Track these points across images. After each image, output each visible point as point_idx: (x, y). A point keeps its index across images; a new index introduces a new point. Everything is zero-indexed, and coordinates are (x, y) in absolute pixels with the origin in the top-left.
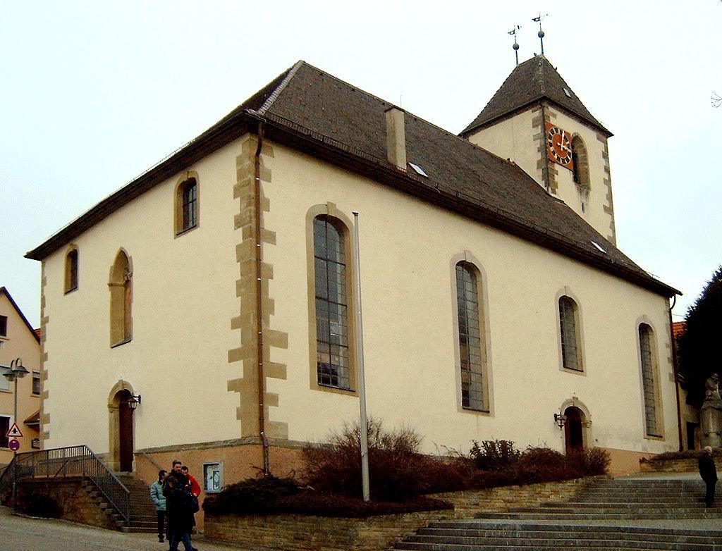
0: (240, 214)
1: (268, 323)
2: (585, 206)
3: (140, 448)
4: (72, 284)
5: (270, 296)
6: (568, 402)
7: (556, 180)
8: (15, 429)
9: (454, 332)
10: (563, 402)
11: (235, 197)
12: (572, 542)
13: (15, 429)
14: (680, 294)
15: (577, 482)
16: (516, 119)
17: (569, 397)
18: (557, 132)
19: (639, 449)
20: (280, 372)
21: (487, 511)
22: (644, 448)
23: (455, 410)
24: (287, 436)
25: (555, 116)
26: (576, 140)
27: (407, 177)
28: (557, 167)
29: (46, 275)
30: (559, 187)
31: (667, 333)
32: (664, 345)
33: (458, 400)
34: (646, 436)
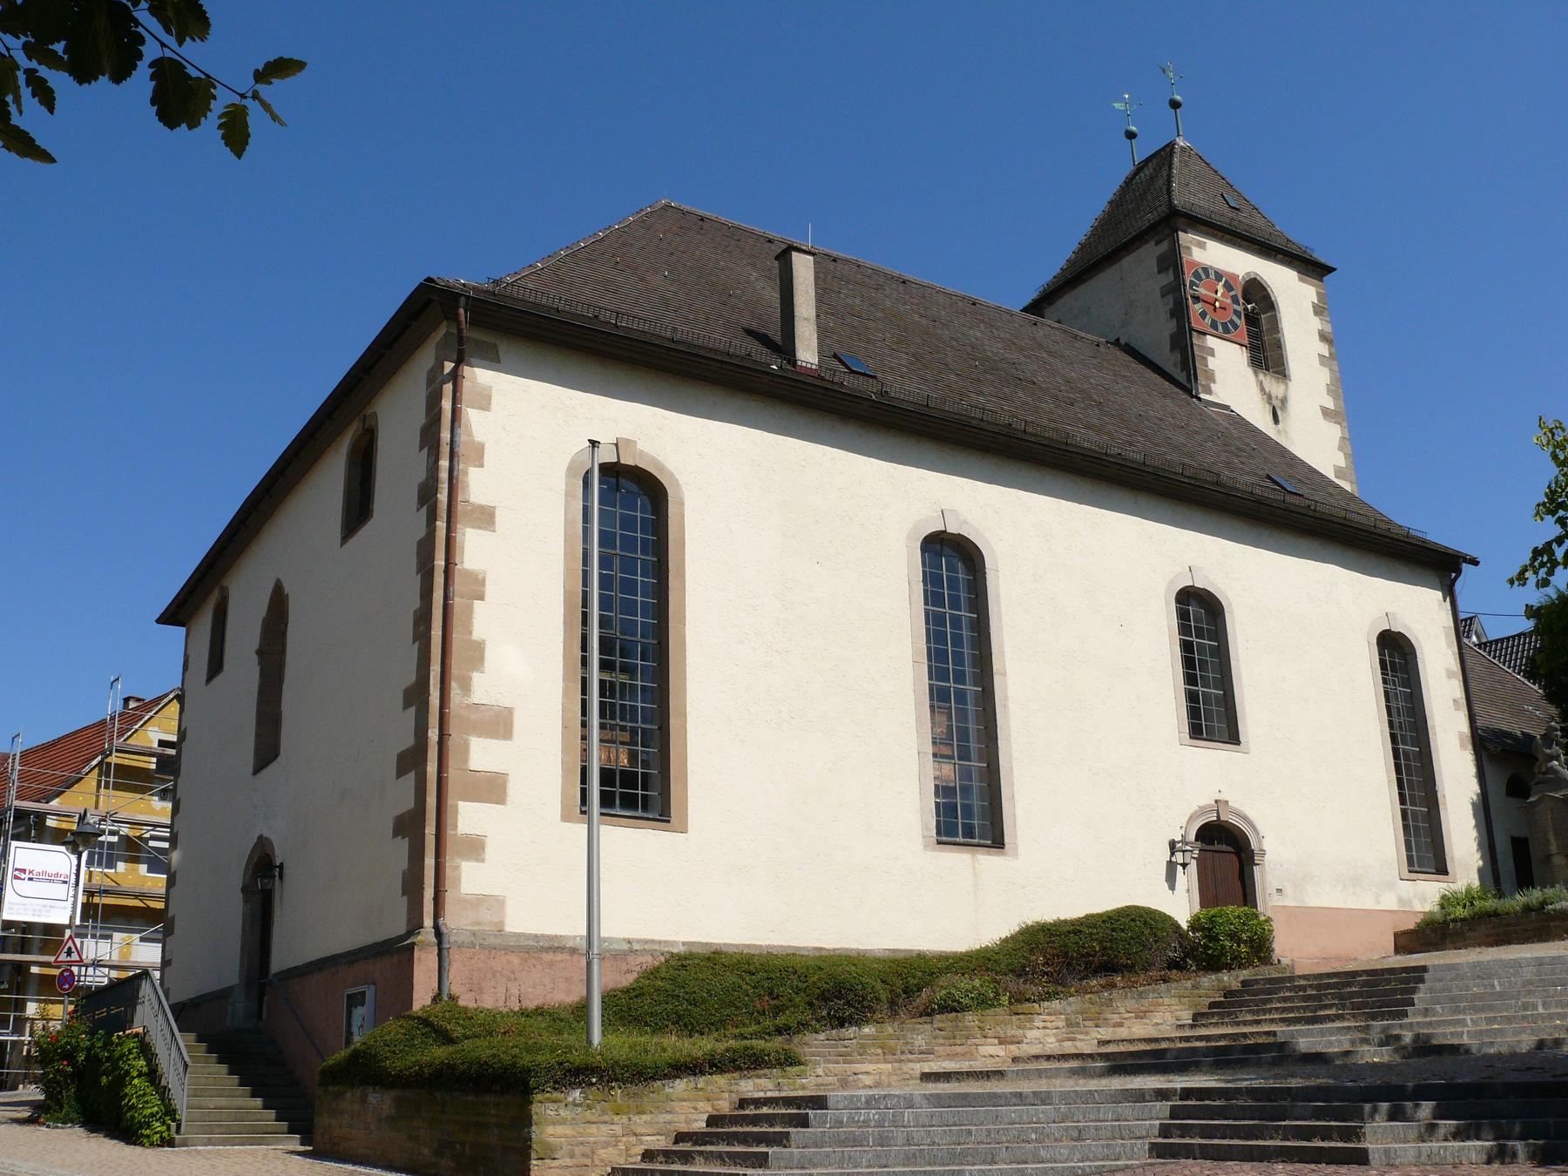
0: (426, 479)
1: (466, 687)
2: (1279, 413)
3: (276, 971)
4: (216, 665)
5: (478, 633)
6: (1202, 811)
7: (1211, 366)
8: (70, 949)
9: (916, 681)
10: (1192, 811)
11: (421, 448)
12: (1035, 1131)
13: (70, 949)
14: (1474, 562)
15: (1195, 987)
16: (1128, 262)
17: (1207, 800)
18: (1208, 276)
19: (1390, 902)
20: (492, 789)
21: (1321, 1081)
22: (1401, 901)
23: (918, 842)
24: (502, 923)
25: (1202, 246)
26: (1255, 292)
27: (823, 379)
28: (1211, 341)
29: (189, 651)
30: (1217, 379)
31: (1449, 646)
32: (1444, 673)
33: (926, 827)
34: (1406, 875)
